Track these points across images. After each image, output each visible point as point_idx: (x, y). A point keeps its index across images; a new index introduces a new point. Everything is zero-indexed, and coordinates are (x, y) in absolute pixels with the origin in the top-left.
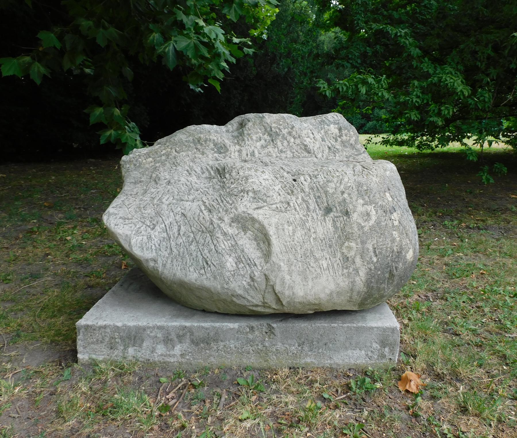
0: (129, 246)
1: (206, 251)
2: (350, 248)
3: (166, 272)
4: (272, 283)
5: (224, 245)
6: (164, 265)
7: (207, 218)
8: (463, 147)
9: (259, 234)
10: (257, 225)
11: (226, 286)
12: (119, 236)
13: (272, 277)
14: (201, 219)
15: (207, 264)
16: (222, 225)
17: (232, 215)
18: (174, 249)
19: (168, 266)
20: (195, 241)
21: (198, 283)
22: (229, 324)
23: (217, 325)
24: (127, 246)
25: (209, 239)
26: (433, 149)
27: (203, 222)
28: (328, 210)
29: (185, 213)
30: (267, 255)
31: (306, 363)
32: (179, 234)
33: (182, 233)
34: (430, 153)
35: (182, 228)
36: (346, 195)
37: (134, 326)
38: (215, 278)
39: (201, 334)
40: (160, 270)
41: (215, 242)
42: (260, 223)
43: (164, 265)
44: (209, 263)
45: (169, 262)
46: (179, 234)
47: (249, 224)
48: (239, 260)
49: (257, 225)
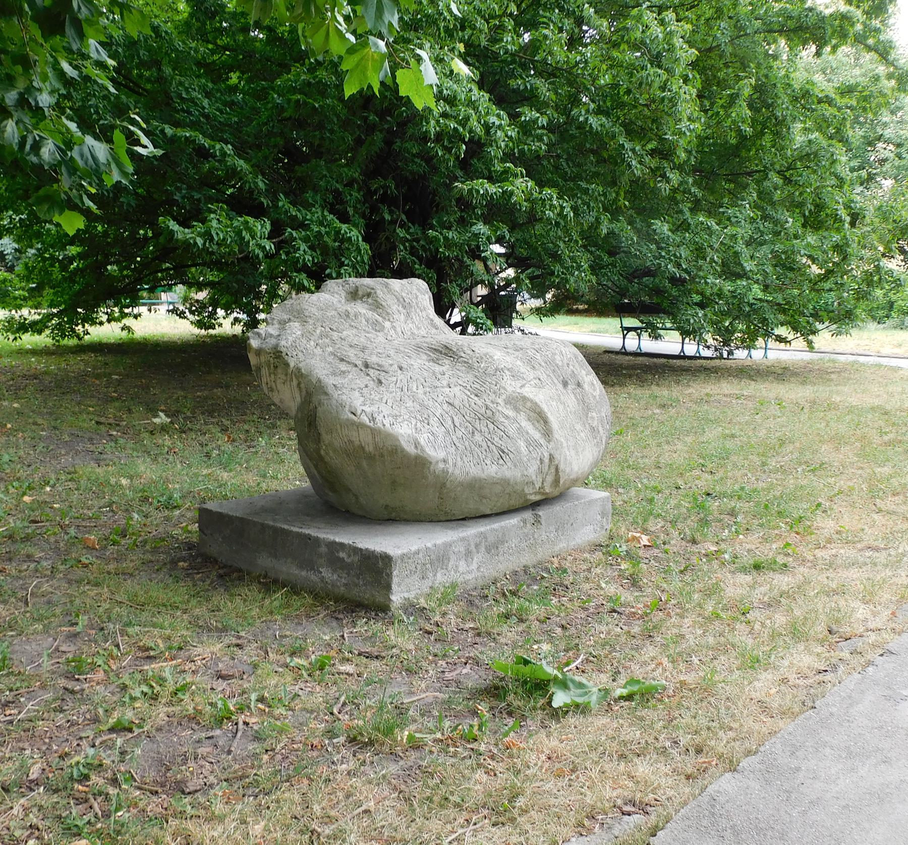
0: (416, 447)
1: (497, 439)
2: (592, 418)
3: (457, 472)
4: (556, 462)
5: (512, 430)
6: (455, 465)
7: (479, 403)
8: (124, 334)
9: (532, 414)
10: (529, 404)
11: (526, 473)
12: (400, 439)
13: (556, 456)
14: (473, 404)
15: (504, 452)
16: (500, 408)
17: (504, 397)
18: (458, 444)
19: (459, 463)
20: (476, 432)
21: (499, 475)
22: (512, 521)
23: (503, 523)
24: (413, 447)
25: (491, 426)
26: (80, 339)
27: (476, 408)
28: (565, 384)
29: (451, 401)
30: (547, 433)
31: (560, 550)
32: (455, 426)
33: (457, 424)
34: (78, 346)
35: (455, 419)
36: (571, 367)
37: (443, 543)
38: (515, 466)
39: (491, 539)
40: (450, 471)
41: (502, 428)
42: (532, 401)
43: (455, 465)
44: (506, 451)
45: (459, 459)
46: (455, 426)
47: (520, 405)
48: (528, 445)
49: (529, 404)
